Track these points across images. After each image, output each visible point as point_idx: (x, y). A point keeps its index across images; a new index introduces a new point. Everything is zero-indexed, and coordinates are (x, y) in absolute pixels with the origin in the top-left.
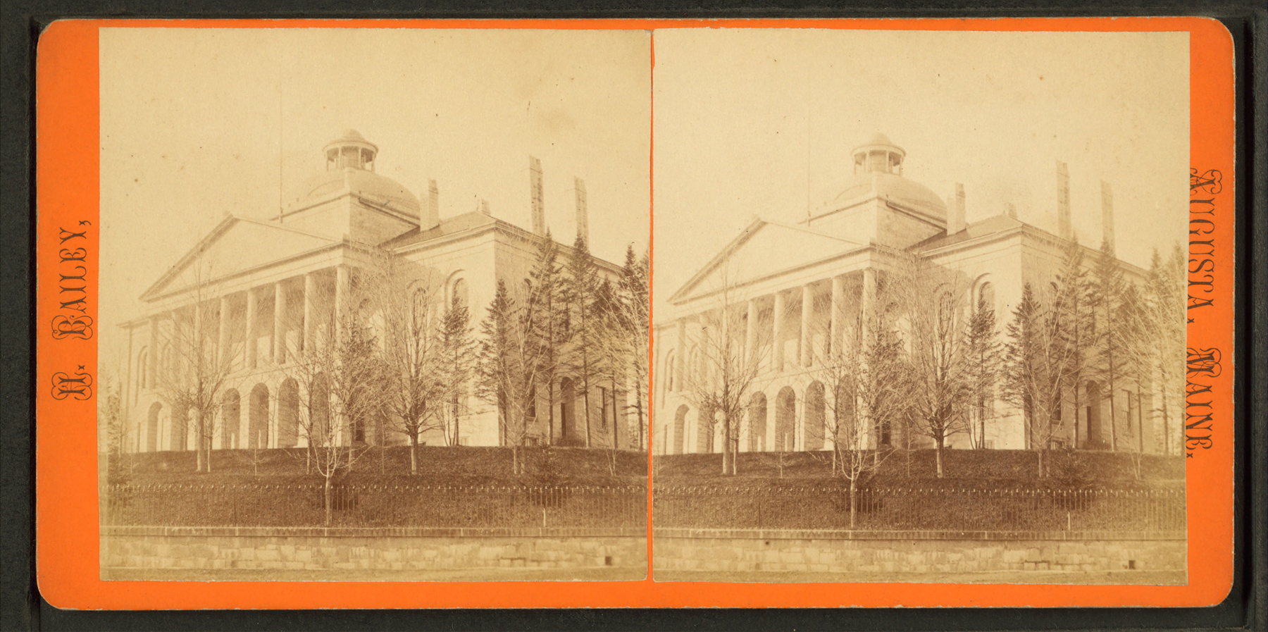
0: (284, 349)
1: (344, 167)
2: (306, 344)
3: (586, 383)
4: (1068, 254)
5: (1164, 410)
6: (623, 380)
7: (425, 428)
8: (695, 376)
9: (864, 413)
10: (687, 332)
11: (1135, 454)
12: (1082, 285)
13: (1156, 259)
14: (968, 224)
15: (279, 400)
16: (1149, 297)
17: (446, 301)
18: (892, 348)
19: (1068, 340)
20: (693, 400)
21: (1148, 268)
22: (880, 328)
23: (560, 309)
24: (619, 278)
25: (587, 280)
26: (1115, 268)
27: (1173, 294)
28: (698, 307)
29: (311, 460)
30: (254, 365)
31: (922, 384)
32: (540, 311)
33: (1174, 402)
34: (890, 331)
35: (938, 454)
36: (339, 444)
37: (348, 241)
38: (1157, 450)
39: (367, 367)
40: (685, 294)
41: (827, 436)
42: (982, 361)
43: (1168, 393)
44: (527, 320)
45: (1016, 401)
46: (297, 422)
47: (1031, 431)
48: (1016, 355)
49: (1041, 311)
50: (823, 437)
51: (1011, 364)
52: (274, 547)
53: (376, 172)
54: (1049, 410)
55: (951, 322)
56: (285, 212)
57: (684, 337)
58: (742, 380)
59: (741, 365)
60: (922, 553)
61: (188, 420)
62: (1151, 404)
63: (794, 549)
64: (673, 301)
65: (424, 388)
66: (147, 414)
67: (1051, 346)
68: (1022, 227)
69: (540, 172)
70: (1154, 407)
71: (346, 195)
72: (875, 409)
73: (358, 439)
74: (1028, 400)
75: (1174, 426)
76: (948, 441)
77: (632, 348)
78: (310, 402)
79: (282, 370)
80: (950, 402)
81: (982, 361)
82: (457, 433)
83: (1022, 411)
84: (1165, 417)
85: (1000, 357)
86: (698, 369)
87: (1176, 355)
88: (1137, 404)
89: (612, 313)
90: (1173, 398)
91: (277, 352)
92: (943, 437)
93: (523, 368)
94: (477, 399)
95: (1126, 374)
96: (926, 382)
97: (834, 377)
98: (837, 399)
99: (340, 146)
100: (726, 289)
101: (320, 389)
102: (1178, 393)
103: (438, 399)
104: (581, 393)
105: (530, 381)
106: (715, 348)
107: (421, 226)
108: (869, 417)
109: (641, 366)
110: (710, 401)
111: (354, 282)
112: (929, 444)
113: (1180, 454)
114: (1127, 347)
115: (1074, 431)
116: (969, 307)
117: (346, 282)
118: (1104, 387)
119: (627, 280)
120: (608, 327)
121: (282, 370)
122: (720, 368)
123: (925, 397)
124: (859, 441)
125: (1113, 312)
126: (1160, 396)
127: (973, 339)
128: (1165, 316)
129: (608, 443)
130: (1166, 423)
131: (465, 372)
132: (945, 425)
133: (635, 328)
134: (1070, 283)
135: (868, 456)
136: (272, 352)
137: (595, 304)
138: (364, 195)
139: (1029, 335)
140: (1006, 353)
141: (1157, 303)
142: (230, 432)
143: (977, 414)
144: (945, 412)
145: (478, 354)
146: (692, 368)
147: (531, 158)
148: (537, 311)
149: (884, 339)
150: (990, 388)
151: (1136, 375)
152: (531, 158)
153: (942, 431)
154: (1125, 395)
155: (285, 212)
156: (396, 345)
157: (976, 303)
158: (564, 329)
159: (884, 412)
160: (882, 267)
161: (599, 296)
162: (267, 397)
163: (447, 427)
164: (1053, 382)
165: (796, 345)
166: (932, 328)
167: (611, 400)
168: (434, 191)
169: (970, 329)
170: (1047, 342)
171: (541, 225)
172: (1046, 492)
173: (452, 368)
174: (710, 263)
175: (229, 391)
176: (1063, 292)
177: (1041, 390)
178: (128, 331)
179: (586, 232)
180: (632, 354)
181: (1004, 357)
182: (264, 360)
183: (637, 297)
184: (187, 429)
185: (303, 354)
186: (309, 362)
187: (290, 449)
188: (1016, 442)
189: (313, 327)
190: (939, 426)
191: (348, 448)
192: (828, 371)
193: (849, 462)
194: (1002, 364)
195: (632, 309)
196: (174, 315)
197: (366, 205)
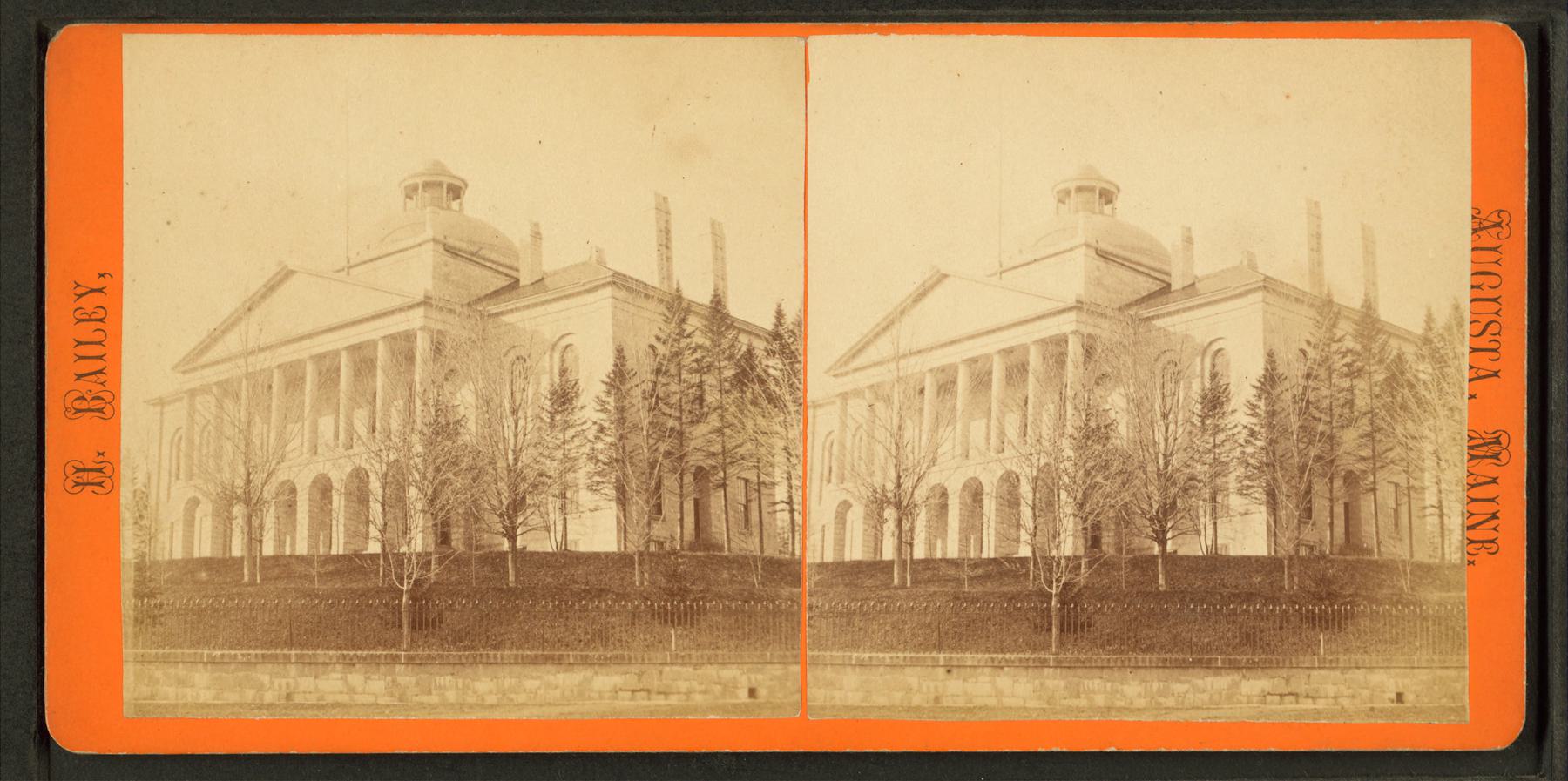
0: (351, 431)
3: (725, 473)
4: (1320, 314)
7: (525, 529)
8: (859, 465)
9: (1069, 510)
10: (850, 410)
11: (1404, 561)
13: (1429, 320)
14: (1196, 277)
19: (1320, 420)
20: (857, 493)
21: (1419, 331)
23: (693, 381)
26: (1379, 331)
27: (1450, 363)
28: (863, 380)
30: (314, 450)
31: (1141, 474)
32: (668, 384)
36: (419, 549)
39: (453, 453)
40: (846, 363)
41: (1022, 539)
43: (1444, 486)
44: (652, 396)
46: (368, 522)
48: (1256, 439)
49: (1287, 384)
51: (1250, 450)
52: (339, 676)
54: (1297, 506)
56: (352, 263)
59: (916, 452)
60: (1140, 684)
61: (233, 519)
63: (334, 675)
64: (832, 373)
65: (524, 479)
71: (427, 241)
72: (1081, 505)
75: (1452, 527)
79: (349, 457)
80: (1175, 496)
81: (1215, 446)
82: (565, 535)
83: (1263, 508)
84: (1441, 516)
85: (1236, 441)
87: (1454, 439)
89: (756, 387)
91: (342, 436)
94: (589, 493)
95: (1392, 462)
98: (1035, 493)
99: (420, 181)
100: (898, 358)
105: (656, 472)
108: (1075, 516)
110: (878, 496)
111: (438, 349)
112: (499, 545)
113: (1459, 561)
115: (1328, 533)
116: (1199, 379)
117: (428, 349)
119: (776, 345)
123: (1143, 490)
124: (1062, 545)
126: (1434, 489)
127: (1203, 419)
128: (1441, 390)
130: (1442, 523)
132: (1169, 525)
134: (1323, 350)
135: (1074, 563)
139: (1272, 414)
143: (1208, 512)
144: (1168, 509)
146: (856, 455)
147: (657, 195)
148: (664, 385)
149: (1093, 419)
150: (1224, 479)
152: (657, 195)
153: (1164, 532)
154: (1392, 488)
155: (352, 262)
157: (1207, 374)
158: (697, 407)
159: (1093, 510)
160: (1090, 330)
163: (1203, 533)
164: (1303, 472)
165: (984, 426)
166: (1152, 406)
170: (1294, 422)
171: (669, 277)
174: (878, 325)
176: (1315, 360)
178: (158, 409)
179: (725, 287)
180: (782, 438)
181: (1241, 441)
182: (327, 445)
183: (788, 367)
185: (374, 437)
186: (383, 447)
187: (358, 555)
188: (1257, 546)
189: (387, 405)
190: (1161, 526)
191: (431, 553)
192: (373, 455)
194: (1239, 450)
195: (781, 382)
196: (215, 390)
197: (452, 253)
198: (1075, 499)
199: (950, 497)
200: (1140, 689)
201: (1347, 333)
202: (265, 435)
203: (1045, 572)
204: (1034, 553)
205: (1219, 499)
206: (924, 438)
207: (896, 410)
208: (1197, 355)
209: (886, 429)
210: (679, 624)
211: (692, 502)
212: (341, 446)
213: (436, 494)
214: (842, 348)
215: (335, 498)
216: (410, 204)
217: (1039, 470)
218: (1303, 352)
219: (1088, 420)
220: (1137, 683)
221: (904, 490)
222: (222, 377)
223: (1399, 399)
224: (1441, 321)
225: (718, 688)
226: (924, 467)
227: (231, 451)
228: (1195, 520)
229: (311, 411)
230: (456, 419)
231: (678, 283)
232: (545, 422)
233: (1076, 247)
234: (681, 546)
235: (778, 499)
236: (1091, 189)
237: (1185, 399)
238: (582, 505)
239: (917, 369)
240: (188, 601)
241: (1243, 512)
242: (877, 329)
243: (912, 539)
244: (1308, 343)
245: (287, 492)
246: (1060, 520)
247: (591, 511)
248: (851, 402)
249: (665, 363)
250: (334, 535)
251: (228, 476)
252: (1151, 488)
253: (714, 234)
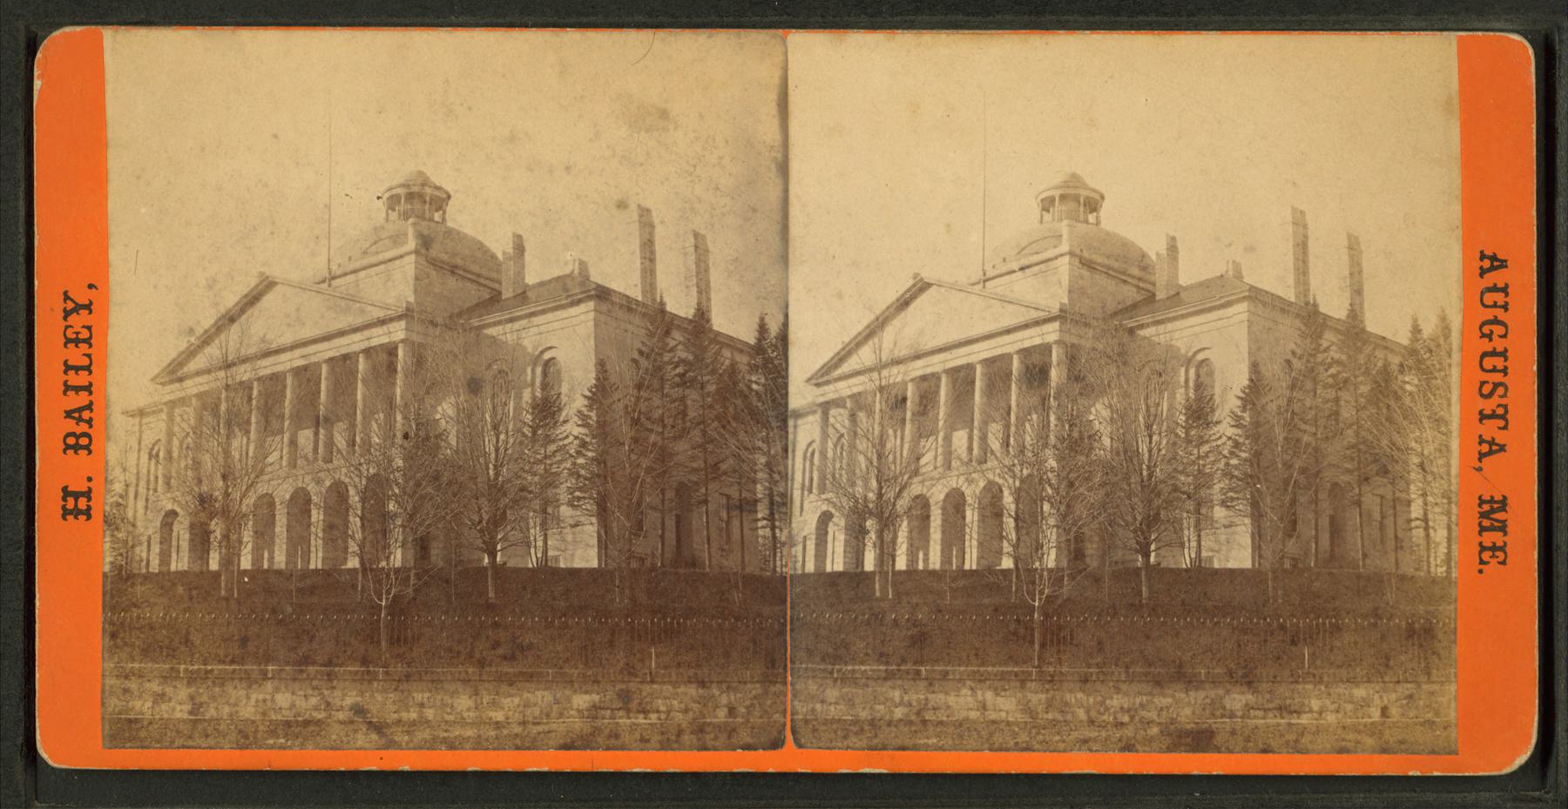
0: (330, 443)
1: (1061, 220)
2: (1012, 441)
3: (1360, 489)
5: (1426, 520)
6: (751, 485)
7: (506, 544)
8: (841, 475)
9: (1052, 521)
10: (832, 420)
12: (671, 362)
13: (1416, 330)
15: (979, 508)
16: (754, 379)
19: (652, 430)
20: (839, 504)
21: (752, 341)
22: (1072, 415)
23: (1329, 396)
24: (748, 358)
26: (1365, 343)
27: (1437, 374)
28: (844, 389)
30: (948, 466)
31: (471, 485)
32: (650, 399)
33: (1437, 510)
34: (1084, 419)
35: (1143, 573)
36: (398, 564)
37: (413, 311)
38: (762, 569)
39: (434, 468)
40: (828, 372)
41: (1005, 550)
43: (1430, 499)
44: (1287, 411)
46: (1001, 538)
47: (1260, 545)
48: (1241, 450)
49: (616, 396)
51: (1234, 461)
53: (1102, 225)
55: (1160, 408)
57: (827, 426)
58: (899, 481)
59: (898, 462)
60: (470, 697)
61: (211, 533)
64: (813, 381)
65: (505, 494)
68: (1250, 290)
69: (1305, 227)
70: (1414, 515)
73: (1076, 558)
74: (1255, 504)
75: (1438, 540)
77: (764, 446)
79: (328, 470)
80: (1159, 508)
81: (546, 457)
82: (545, 552)
83: (1247, 521)
84: (1427, 528)
86: (844, 466)
87: (1440, 451)
88: (1391, 511)
89: (739, 402)
90: (1437, 504)
91: (321, 450)
92: (496, 552)
94: (570, 509)
95: (725, 473)
96: (1129, 485)
97: (1014, 477)
98: (1017, 504)
99: (1057, 193)
100: (880, 367)
101: (1029, 494)
103: (522, 508)
104: (700, 503)
105: (1290, 488)
106: (865, 440)
107: (1157, 293)
110: (859, 506)
111: (419, 362)
113: (1445, 574)
115: (1314, 545)
116: (1182, 390)
118: (697, 491)
119: (759, 360)
120: (734, 419)
121: (328, 470)
123: (1127, 502)
124: (1045, 556)
125: (708, 396)
126: (1420, 501)
127: (1187, 430)
129: (1386, 566)
130: (1428, 536)
132: (499, 537)
134: (1308, 361)
135: (1056, 576)
136: (970, 449)
137: (718, 391)
138: (1086, 254)
139: (602, 424)
141: (1417, 386)
144: (1152, 521)
145: (1226, 452)
146: (838, 465)
147: (1294, 210)
148: (646, 399)
151: (737, 475)
152: (1294, 210)
153: (1149, 545)
154: (1378, 500)
155: (989, 275)
157: (1191, 384)
158: (680, 422)
160: (1075, 340)
161: (1376, 382)
163: (1187, 545)
164: (635, 484)
165: (966, 436)
166: (483, 415)
170: (1279, 434)
174: (860, 334)
176: (1300, 371)
177: (1272, 495)
180: (764, 454)
181: (1226, 452)
182: (307, 459)
183: (1424, 383)
185: (1008, 451)
187: (990, 570)
188: (585, 556)
191: (1063, 569)
192: (1006, 470)
193: (379, 582)
194: (1223, 461)
195: (764, 396)
196: (849, 404)
200: (470, 703)
204: (1016, 564)
206: (906, 446)
207: (877, 421)
209: (868, 439)
213: (415, 510)
214: (826, 356)
215: (968, 513)
216: (1047, 217)
217: (1022, 481)
219: (1071, 431)
220: (467, 697)
222: (202, 389)
223: (731, 410)
224: (1429, 328)
226: (906, 477)
228: (1178, 531)
229: (290, 424)
230: (437, 433)
231: (661, 297)
233: (1062, 255)
235: (1414, 515)
236: (1076, 198)
237: (1168, 410)
238: (1216, 522)
239: (899, 379)
243: (895, 550)
245: (919, 507)
247: (1225, 527)
249: (648, 377)
252: (1135, 500)
253: (1350, 248)
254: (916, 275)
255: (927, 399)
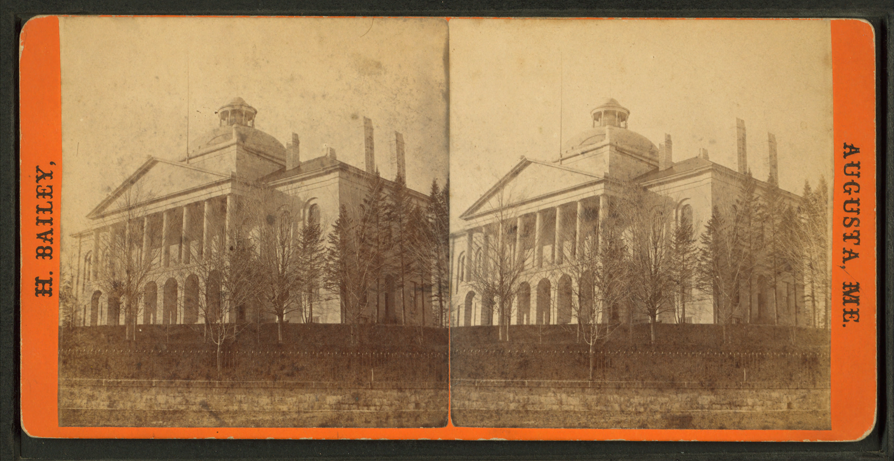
0: (562, 255)
2: (204, 250)
4: (744, 185)
5: (813, 296)
7: (288, 310)
8: (479, 271)
9: (600, 297)
10: (474, 239)
11: (792, 327)
13: (807, 188)
14: (673, 163)
15: (558, 290)
16: (430, 216)
17: (304, 219)
18: (619, 251)
21: (429, 195)
22: (611, 237)
25: (777, 206)
26: (778, 195)
27: (819, 213)
28: (481, 221)
29: (579, 333)
30: (540, 265)
31: (269, 276)
32: (371, 227)
35: (652, 326)
36: (227, 321)
38: (434, 325)
40: (472, 212)
41: (573, 314)
42: (311, 260)
44: (734, 234)
45: (708, 289)
46: (571, 306)
48: (708, 257)
49: (351, 226)
50: (570, 315)
54: (731, 296)
55: (661, 233)
56: (563, 157)
58: (513, 274)
60: (268, 397)
61: (120, 303)
62: (804, 292)
64: (464, 217)
65: (288, 282)
66: (464, 299)
67: (360, 250)
69: (744, 129)
70: (806, 294)
71: (233, 144)
72: (607, 294)
73: (613, 318)
74: (715, 287)
75: (820, 308)
76: (286, 317)
77: (436, 254)
78: (580, 292)
79: (187, 268)
80: (661, 289)
82: (311, 314)
83: (711, 297)
84: (813, 301)
85: (696, 258)
87: (821, 257)
89: (421, 229)
90: (819, 287)
92: (283, 314)
93: (358, 268)
94: (325, 290)
95: (413, 270)
96: (644, 276)
97: (578, 272)
98: (580, 287)
99: (602, 110)
100: (502, 209)
101: (587, 282)
102: (823, 283)
103: (297, 290)
106: (493, 251)
108: (603, 300)
109: (442, 267)
110: (490, 288)
111: (239, 206)
112: (645, 319)
114: (786, 251)
116: (674, 222)
117: (233, 207)
119: (433, 205)
120: (419, 239)
121: (187, 268)
122: (498, 265)
124: (596, 317)
126: (810, 286)
127: (677, 245)
128: (813, 229)
129: (790, 322)
130: (814, 305)
131: (318, 270)
132: (285, 306)
133: (438, 240)
134: (746, 206)
135: (602, 328)
136: (180, 256)
140: (700, 255)
142: (523, 313)
143: (680, 299)
144: (657, 297)
146: (478, 265)
147: (738, 119)
148: (368, 228)
149: (614, 245)
150: (689, 280)
151: (420, 271)
153: (655, 310)
154: (786, 285)
155: (564, 157)
156: (268, 251)
159: (242, 297)
160: (613, 194)
161: (784, 218)
162: (550, 288)
163: (677, 310)
164: (362, 276)
165: (551, 248)
166: (275, 236)
167: (793, 291)
168: (669, 141)
169: (674, 238)
170: (729, 247)
171: (745, 166)
172: (357, 354)
173: (308, 267)
174: (490, 190)
175: (523, 283)
176: (741, 211)
177: (725, 282)
178: (78, 239)
179: (776, 173)
180: (436, 259)
182: (175, 262)
184: (493, 311)
186: (207, 262)
187: (565, 325)
188: (334, 317)
189: (582, 241)
190: (653, 307)
192: (574, 268)
193: (216, 331)
194: (697, 263)
196: (484, 230)
197: (621, 152)
198: (603, 291)
199: (532, 289)
200: (268, 401)
201: (760, 196)
202: (139, 255)
203: (586, 333)
204: (579, 322)
205: (313, 291)
206: (517, 254)
207: (500, 240)
208: (674, 208)
210: (376, 366)
211: (384, 295)
212: (183, 261)
213: (237, 291)
214: (471, 203)
215: (552, 293)
216: (597, 123)
217: (583, 274)
218: (734, 206)
219: (611, 246)
220: (266, 397)
221: (505, 286)
222: (115, 222)
224: (814, 188)
225: (769, 403)
226: (516, 272)
227: (492, 265)
232: (673, 249)
234: (750, 320)
235: (806, 294)
236: (614, 113)
237: (666, 234)
239: (512, 216)
240: (94, 350)
241: (700, 298)
242: (490, 192)
243: (510, 313)
244: (737, 201)
245: (524, 289)
246: (595, 303)
248: (475, 235)
250: (552, 313)
251: (491, 280)
252: (647, 285)
254: (522, 157)
255: (529, 228)
